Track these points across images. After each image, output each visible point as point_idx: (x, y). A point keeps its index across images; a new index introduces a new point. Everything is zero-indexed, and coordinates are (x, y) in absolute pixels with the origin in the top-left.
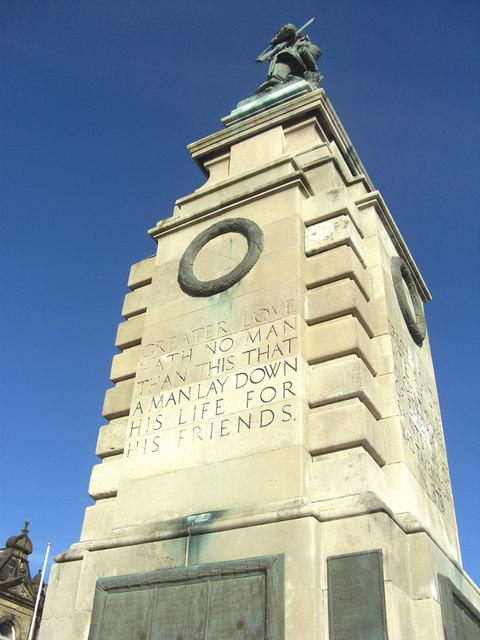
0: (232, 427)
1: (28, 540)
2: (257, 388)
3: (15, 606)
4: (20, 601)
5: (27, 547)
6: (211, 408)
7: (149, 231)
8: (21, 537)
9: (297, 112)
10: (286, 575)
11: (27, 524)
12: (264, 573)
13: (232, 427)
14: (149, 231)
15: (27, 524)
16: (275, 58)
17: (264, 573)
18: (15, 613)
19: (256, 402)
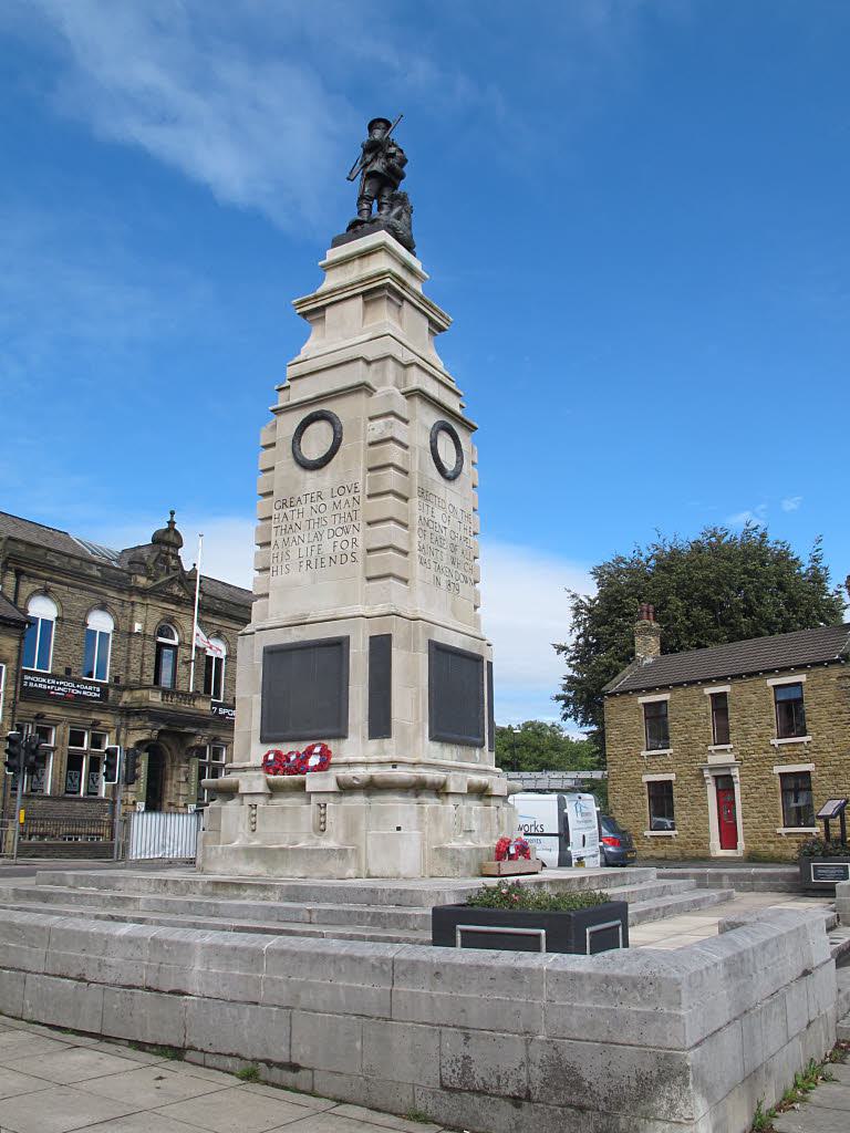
0: (327, 561)
1: (177, 533)
2: (339, 539)
3: (173, 607)
4: (178, 601)
5: (176, 541)
6: (315, 549)
7: (320, 263)
8: (167, 531)
9: (769, 870)
10: (350, 683)
11: (172, 513)
12: (339, 645)
13: (327, 561)
14: (320, 263)
15: (172, 513)
16: (145, 746)
17: (339, 645)
18: (175, 614)
19: (338, 548)
